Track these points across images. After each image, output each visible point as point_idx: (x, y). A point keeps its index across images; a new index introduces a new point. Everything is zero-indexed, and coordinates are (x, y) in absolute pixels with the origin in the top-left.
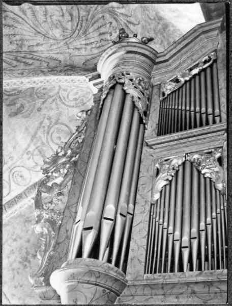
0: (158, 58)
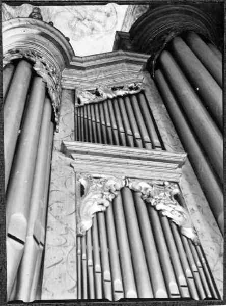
0: (72, 61)
